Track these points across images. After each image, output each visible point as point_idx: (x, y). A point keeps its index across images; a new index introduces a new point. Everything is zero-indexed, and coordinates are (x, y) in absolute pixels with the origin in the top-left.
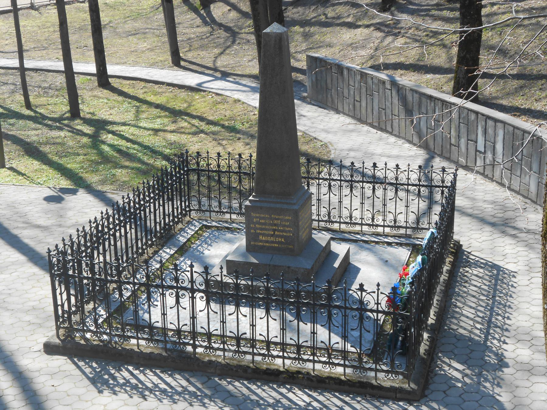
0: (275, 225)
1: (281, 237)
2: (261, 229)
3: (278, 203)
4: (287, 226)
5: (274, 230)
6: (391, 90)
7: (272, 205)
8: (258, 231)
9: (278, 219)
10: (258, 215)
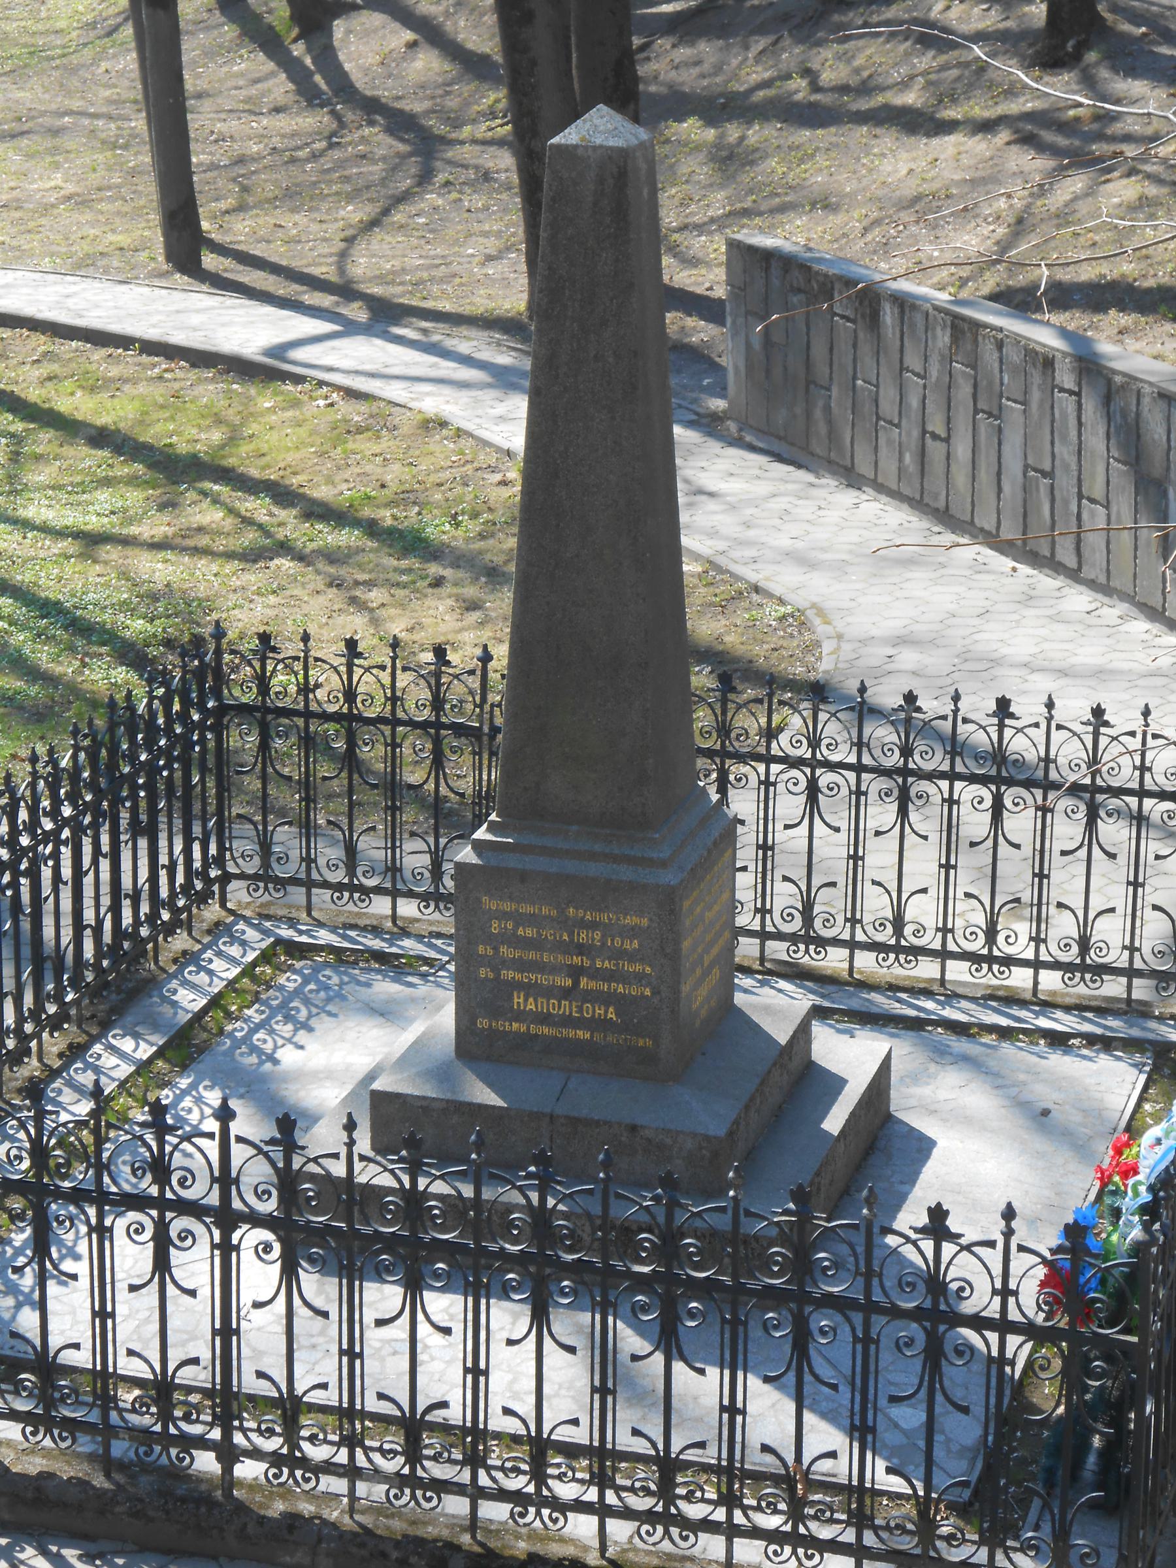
0: (581, 950)
1: (606, 999)
2: (522, 966)
3: (593, 856)
4: (632, 957)
5: (576, 973)
6: (1078, 394)
7: (571, 866)
8: (509, 974)
9: (593, 926)
10: (508, 906)
